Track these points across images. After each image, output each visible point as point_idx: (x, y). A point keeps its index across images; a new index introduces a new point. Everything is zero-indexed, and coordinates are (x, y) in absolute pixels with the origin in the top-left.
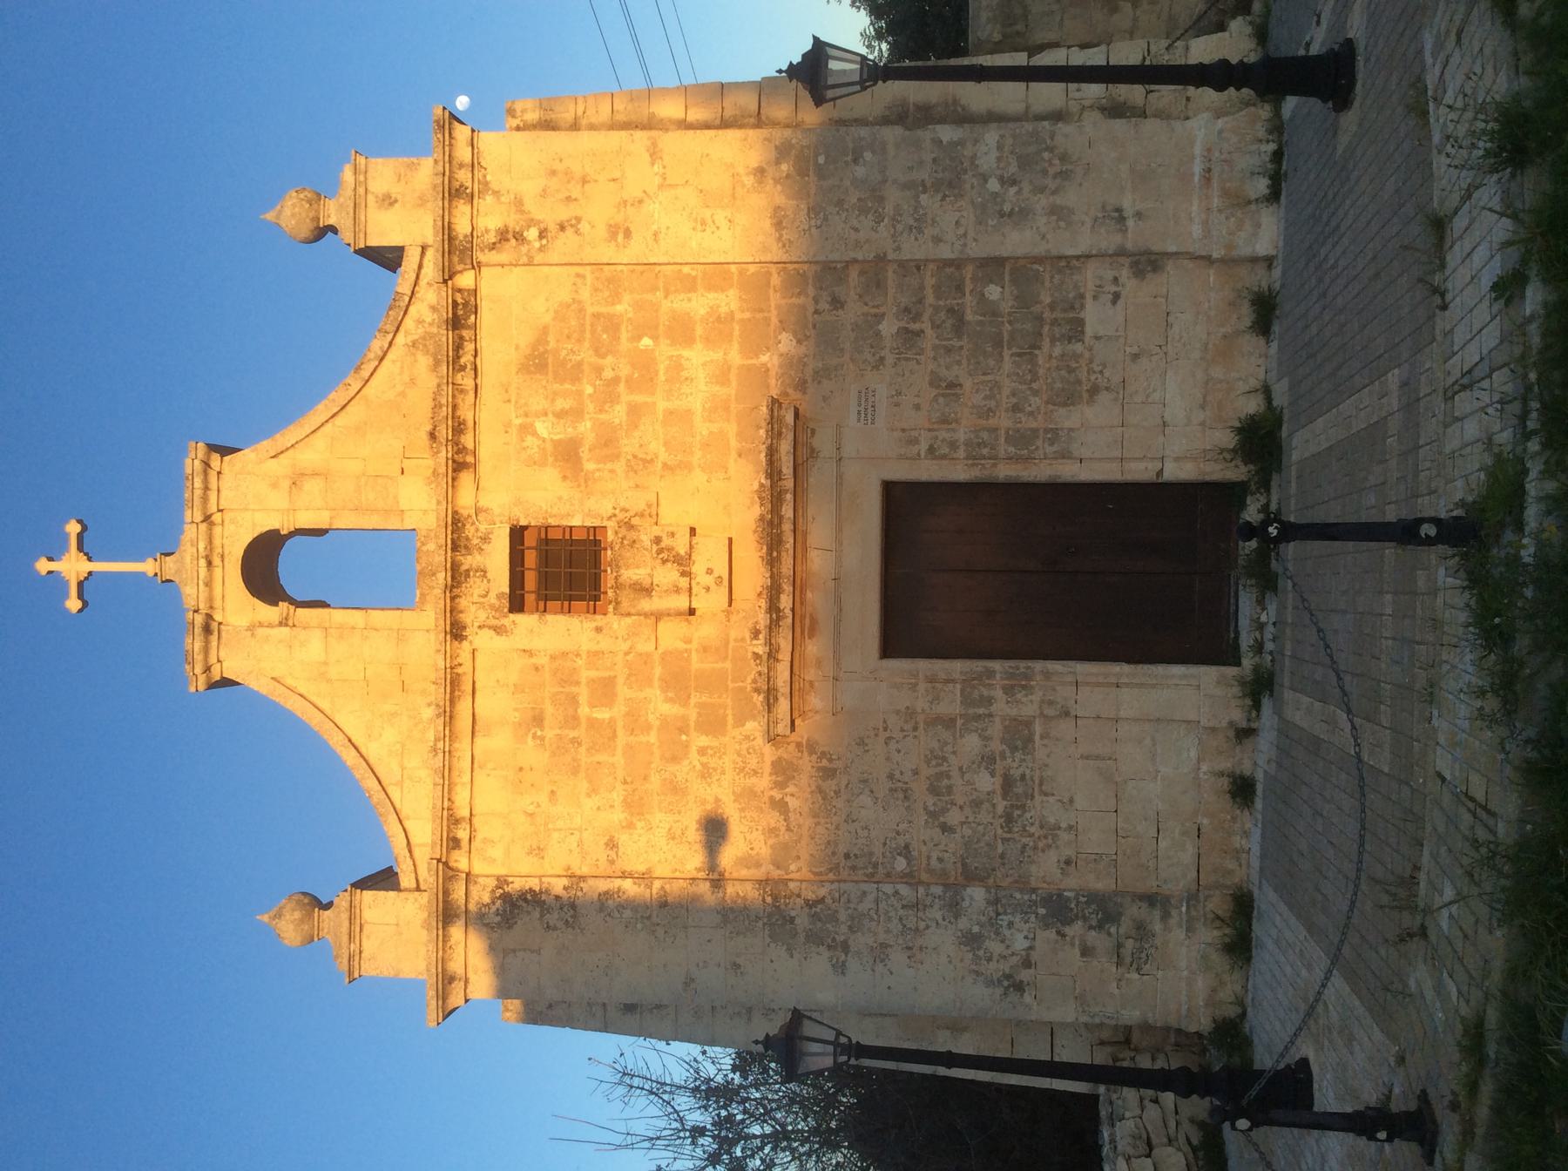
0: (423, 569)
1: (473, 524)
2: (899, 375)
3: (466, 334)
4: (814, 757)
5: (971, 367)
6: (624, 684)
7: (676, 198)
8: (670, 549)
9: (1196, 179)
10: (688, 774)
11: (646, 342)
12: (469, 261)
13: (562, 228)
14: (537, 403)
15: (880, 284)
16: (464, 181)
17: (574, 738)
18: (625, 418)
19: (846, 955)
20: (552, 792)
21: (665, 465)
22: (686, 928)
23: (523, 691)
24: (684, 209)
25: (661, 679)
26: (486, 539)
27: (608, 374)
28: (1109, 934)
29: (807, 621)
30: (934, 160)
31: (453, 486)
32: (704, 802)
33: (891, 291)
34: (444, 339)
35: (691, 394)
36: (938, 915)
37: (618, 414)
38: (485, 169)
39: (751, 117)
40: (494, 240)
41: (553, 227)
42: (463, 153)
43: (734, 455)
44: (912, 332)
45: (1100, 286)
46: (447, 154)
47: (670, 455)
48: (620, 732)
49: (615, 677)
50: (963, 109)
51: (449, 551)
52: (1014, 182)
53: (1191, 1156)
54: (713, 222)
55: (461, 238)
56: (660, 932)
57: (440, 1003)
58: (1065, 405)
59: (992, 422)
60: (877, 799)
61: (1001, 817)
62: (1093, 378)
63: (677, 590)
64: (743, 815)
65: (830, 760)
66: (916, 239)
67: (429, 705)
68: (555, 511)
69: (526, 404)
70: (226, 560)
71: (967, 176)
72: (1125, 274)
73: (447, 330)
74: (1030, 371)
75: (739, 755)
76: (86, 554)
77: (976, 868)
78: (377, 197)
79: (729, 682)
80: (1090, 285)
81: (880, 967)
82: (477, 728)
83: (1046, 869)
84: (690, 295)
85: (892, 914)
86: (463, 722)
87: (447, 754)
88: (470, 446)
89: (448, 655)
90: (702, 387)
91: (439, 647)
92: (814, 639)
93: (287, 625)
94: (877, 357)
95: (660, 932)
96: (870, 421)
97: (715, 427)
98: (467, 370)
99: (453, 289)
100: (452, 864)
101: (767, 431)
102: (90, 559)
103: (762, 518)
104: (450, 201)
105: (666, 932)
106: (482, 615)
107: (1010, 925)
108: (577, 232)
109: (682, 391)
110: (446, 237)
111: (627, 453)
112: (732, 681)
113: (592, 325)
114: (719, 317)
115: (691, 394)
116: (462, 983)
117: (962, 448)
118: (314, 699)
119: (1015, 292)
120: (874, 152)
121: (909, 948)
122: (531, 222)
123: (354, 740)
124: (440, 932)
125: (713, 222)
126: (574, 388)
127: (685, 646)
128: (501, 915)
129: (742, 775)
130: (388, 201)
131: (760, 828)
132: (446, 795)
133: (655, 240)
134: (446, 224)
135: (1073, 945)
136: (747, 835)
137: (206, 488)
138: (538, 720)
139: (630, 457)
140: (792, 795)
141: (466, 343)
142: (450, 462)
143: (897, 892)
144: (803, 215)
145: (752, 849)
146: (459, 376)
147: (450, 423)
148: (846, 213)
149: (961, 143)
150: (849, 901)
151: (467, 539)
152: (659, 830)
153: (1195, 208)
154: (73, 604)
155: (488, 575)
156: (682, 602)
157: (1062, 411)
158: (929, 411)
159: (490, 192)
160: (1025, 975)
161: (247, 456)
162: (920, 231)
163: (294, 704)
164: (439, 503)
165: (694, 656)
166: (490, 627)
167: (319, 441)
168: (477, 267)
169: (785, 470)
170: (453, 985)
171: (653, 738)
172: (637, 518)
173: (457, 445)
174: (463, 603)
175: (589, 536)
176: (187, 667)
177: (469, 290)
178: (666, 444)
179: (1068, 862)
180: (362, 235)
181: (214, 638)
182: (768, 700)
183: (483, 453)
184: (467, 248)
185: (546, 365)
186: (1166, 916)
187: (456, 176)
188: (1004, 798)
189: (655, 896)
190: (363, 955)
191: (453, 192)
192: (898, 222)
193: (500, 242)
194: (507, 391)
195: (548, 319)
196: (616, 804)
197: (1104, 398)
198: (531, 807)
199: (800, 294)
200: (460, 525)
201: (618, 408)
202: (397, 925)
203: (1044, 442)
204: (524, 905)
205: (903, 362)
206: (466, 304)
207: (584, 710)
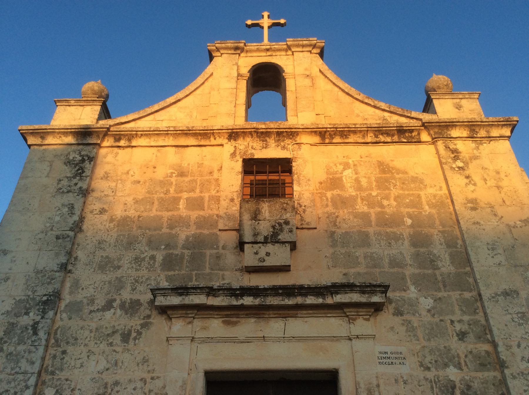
4: (139, 327)
8: (282, 230)
10: (139, 250)
12: (436, 136)
13: (467, 177)
15: (483, 366)
17: (170, 191)
23: (198, 167)
25: (201, 233)
26: (284, 148)
31: (312, 132)
33: (479, 374)
35: (381, 246)
38: (489, 143)
41: (467, 173)
42: (495, 132)
46: (493, 123)
49: (204, 210)
51: (277, 130)
54: (496, 255)
56: (41, 236)
64: (107, 283)
68: (301, 178)
73: (397, 127)
75: (147, 279)
79: (196, 272)
84: (444, 244)
85: (13, 385)
86: (183, 141)
87: (167, 132)
88: (335, 141)
89: (220, 131)
90: (386, 252)
93: (238, 76)
94: (430, 365)
95: (41, 236)
97: (361, 260)
98: (376, 139)
99: (420, 129)
100: (106, 138)
105: (40, 239)
108: (467, 184)
111: (339, 212)
112: (196, 274)
113: (412, 194)
123: (179, 102)
124: (69, 130)
125: (496, 255)
126: (374, 186)
128: (73, 159)
129: (133, 281)
131: (95, 294)
132: (144, 133)
136: (93, 286)
137: (303, 46)
140: (114, 314)
141: (390, 138)
142: (325, 130)
146: (372, 135)
150: (30, 352)
151: (283, 141)
154: (249, 22)
155: (264, 149)
161: (320, 62)
163: (200, 80)
164: (303, 125)
165: (215, 251)
167: (330, 86)
170: (39, 139)
172: (300, 218)
173: (334, 134)
174: (249, 139)
175: (287, 194)
180: (437, 97)
181: (233, 52)
183: (331, 148)
187: (482, 129)
190: (68, 107)
191: (473, 128)
200: (291, 137)
204: (76, 169)
205: (429, 386)
206: (412, 137)
207: (185, 195)
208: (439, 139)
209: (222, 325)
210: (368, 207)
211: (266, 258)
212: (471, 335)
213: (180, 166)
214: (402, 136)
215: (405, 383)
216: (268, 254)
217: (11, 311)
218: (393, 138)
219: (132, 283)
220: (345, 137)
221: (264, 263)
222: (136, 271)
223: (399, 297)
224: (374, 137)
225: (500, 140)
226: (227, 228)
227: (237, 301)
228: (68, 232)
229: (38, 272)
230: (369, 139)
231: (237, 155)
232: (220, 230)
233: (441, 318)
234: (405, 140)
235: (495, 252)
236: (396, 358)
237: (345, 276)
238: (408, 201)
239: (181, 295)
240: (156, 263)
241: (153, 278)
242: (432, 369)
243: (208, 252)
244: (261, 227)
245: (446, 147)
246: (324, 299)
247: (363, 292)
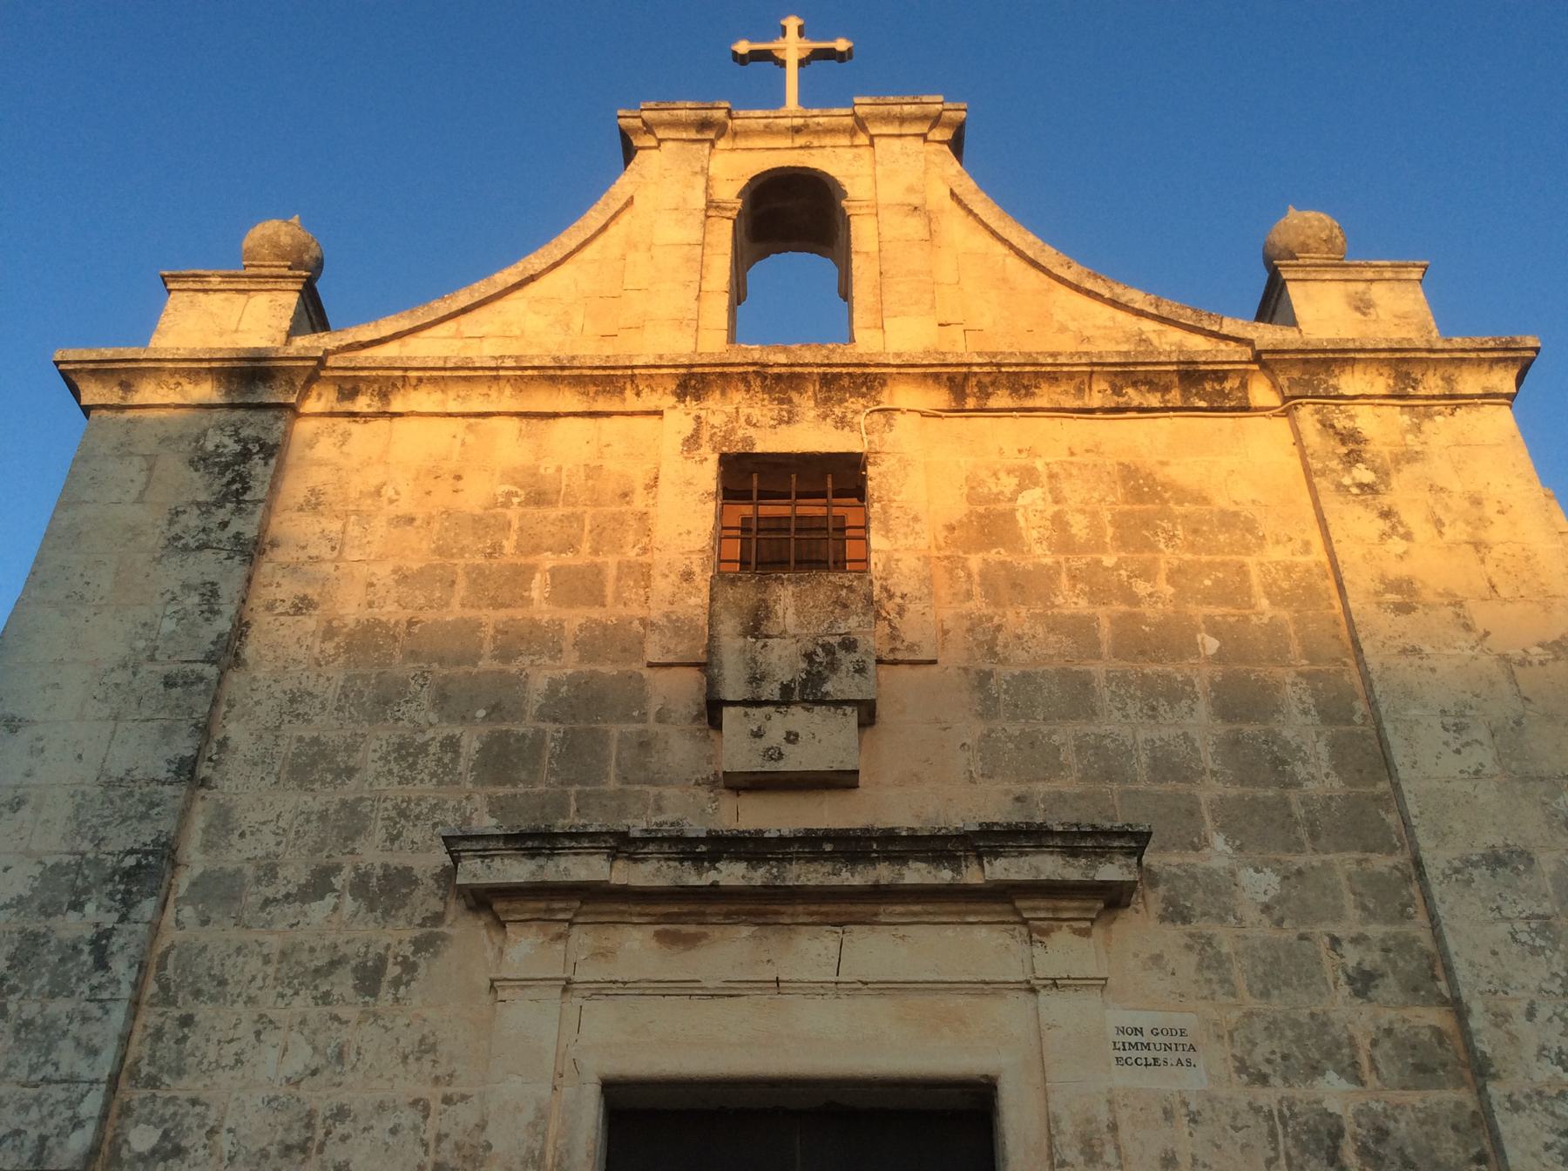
2: (1234, 1118)
4: (408, 950)
8: (833, 666)
12: (1296, 392)
13: (1386, 514)
17: (501, 547)
20: (412, 520)
22: (116, 718)
23: (588, 477)
26: (842, 423)
31: (925, 375)
33: (1414, 1098)
35: (1126, 716)
38: (1452, 414)
40: (1338, 425)
42: (1470, 382)
43: (1020, 789)
44: (1336, 1148)
51: (821, 370)
54: (1467, 744)
55: (1331, 382)
56: (121, 677)
60: (297, 1083)
63: (756, 679)
64: (314, 817)
66: (1548, 1147)
68: (894, 512)
70: (802, 152)
73: (1179, 363)
75: (434, 808)
79: (578, 787)
85: (34, 1114)
86: (542, 400)
87: (494, 373)
88: (993, 403)
90: (1142, 735)
93: (708, 207)
94: (1266, 1069)
95: (121, 677)
96: (1124, 1055)
97: (1068, 756)
98: (1116, 398)
99: (1246, 371)
100: (315, 389)
105: (117, 685)
108: (1384, 536)
111: (1004, 615)
112: (579, 793)
113: (1223, 564)
114: (1284, 762)
116: (116, 401)
118: (600, 240)
122: (1383, 474)
125: (1467, 744)
126: (1108, 540)
129: (393, 814)
132: (428, 374)
136: (272, 826)
140: (335, 909)
142: (965, 370)
143: (77, 1124)
146: (1104, 386)
150: (85, 1019)
152: (313, 676)
154: (743, 47)
155: (784, 426)
156: (733, 687)
161: (953, 167)
164: (898, 355)
167: (982, 241)
170: (116, 389)
172: (888, 630)
173: (993, 383)
174: (738, 396)
177: (1247, 399)
180: (1300, 276)
181: (693, 135)
183: (982, 423)
185: (1142, 501)
187: (1430, 373)
190: (200, 295)
191: (1405, 368)
200: (864, 389)
204: (225, 480)
205: (1265, 1129)
206: (1223, 394)
208: (1304, 401)
209: (654, 944)
210: (1090, 602)
211: (787, 749)
212: (1391, 980)
214: (1194, 391)
215: (1193, 1120)
216: (792, 738)
217: (31, 899)
218: (1167, 397)
219: (389, 818)
220: (1023, 391)
221: (782, 763)
223: (1179, 866)
224: (1109, 392)
226: (670, 659)
228: (198, 667)
229: (109, 785)
230: (1096, 400)
232: (651, 665)
233: (1302, 930)
234: (1203, 404)
235: (1465, 738)
236: (1167, 1047)
238: (1208, 582)
239: (533, 856)
241: (451, 804)
242: (1272, 1080)
243: (615, 730)
244: (773, 658)
246: (957, 870)
247: (1073, 852)
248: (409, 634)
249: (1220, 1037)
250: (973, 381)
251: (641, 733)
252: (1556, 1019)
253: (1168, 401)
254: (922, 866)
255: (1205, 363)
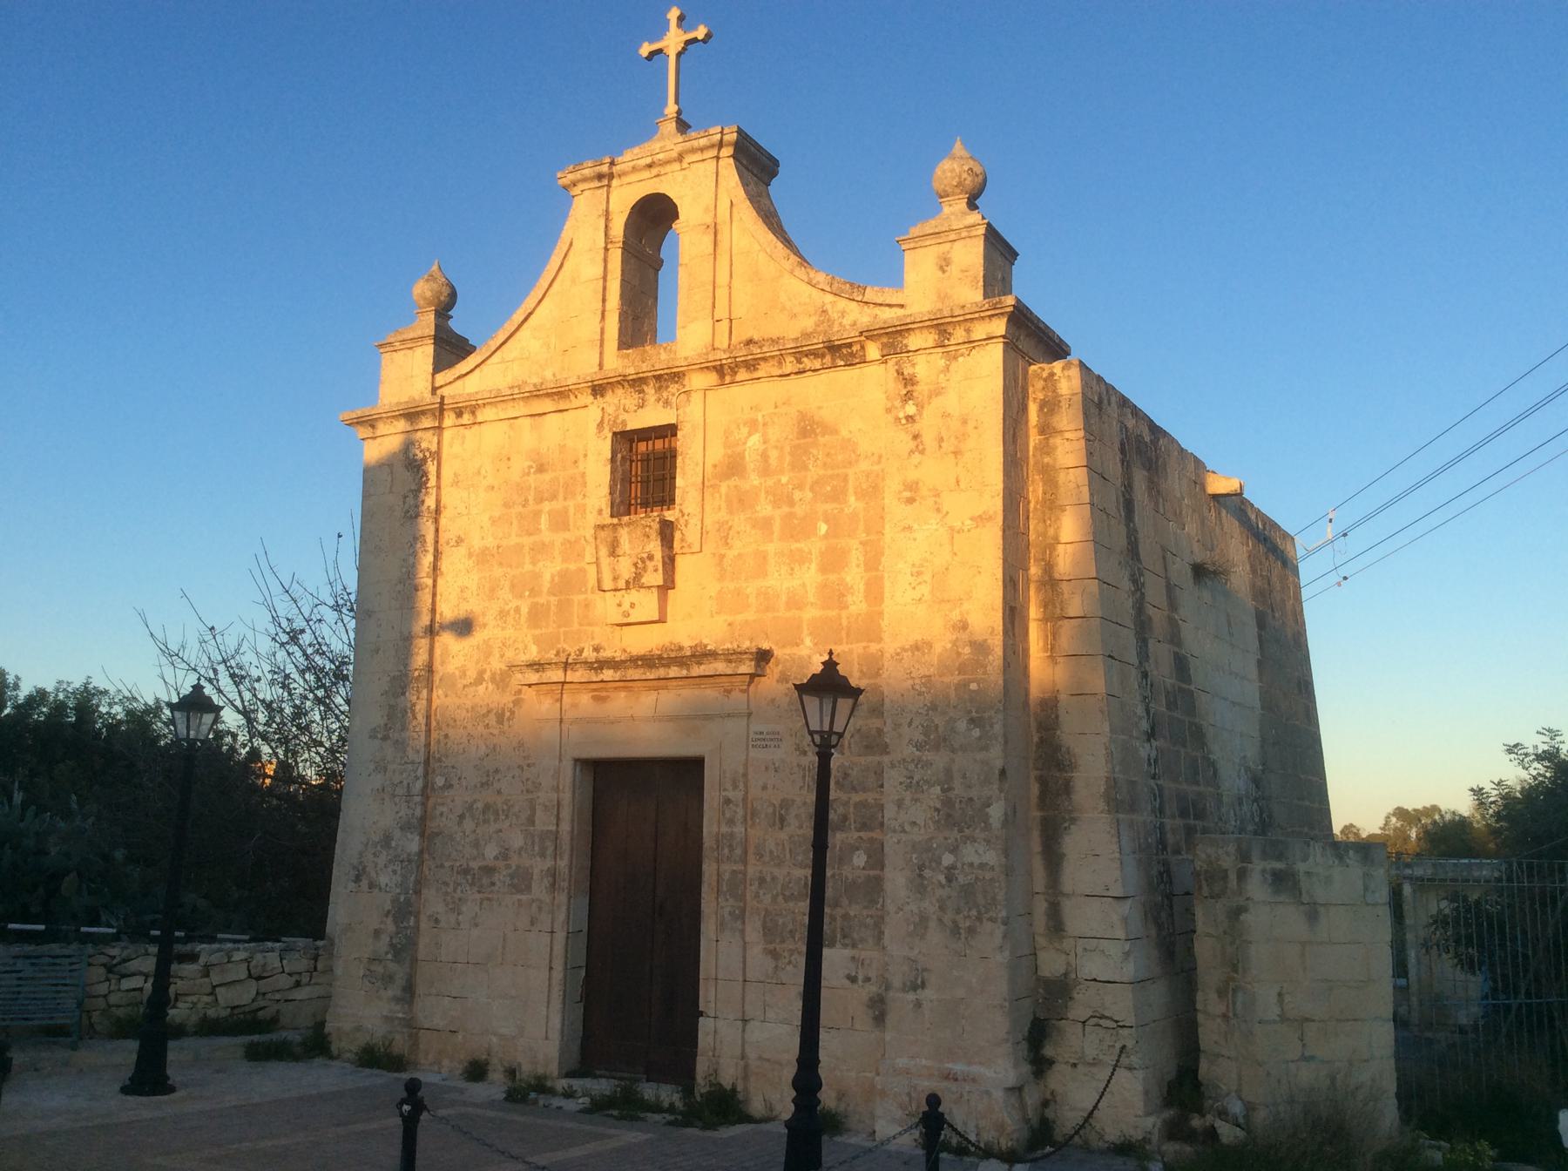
0: (647, 352)
1: (678, 390)
3: (828, 359)
5: (796, 838)
6: (565, 539)
7: (941, 545)
8: (645, 569)
9: (950, 1065)
11: (823, 528)
13: (916, 437)
14: (774, 433)
16: (955, 336)
18: (760, 515)
19: (381, 739)
20: (493, 487)
21: (722, 556)
23: (560, 453)
24: (931, 553)
25: (567, 569)
26: (667, 403)
27: (797, 495)
28: (387, 953)
29: (604, 694)
30: (971, 799)
31: (701, 368)
32: (484, 614)
33: (862, 760)
34: (815, 341)
36: (402, 813)
37: (765, 509)
38: (968, 355)
39: (1062, 610)
40: (905, 373)
42: (980, 331)
43: (730, 619)
45: (862, 964)
47: (731, 560)
48: (532, 539)
49: (569, 530)
50: (1065, 828)
52: (949, 879)
53: (247, 1009)
54: (920, 583)
56: (400, 587)
57: (355, 421)
58: (764, 927)
59: (751, 858)
61: (468, 865)
62: (786, 954)
63: (615, 579)
65: (509, 719)
66: (901, 783)
67: (554, 375)
68: (687, 461)
69: (773, 422)
71: (956, 832)
72: (873, 989)
73: (823, 342)
74: (792, 894)
76: (684, 49)
77: (435, 844)
78: (948, 252)
80: (864, 954)
81: (372, 766)
82: (537, 418)
83: (433, 902)
84: (862, 566)
85: (404, 775)
87: (511, 397)
88: (739, 377)
91: (582, 377)
92: (591, 701)
95: (400, 587)
101: (728, 650)
102: (679, 55)
103: (681, 648)
104: (932, 326)
105: (399, 592)
106: (610, 410)
107: (395, 872)
108: (912, 452)
109: (782, 566)
110: (899, 328)
111: (733, 520)
113: (838, 475)
115: (780, 575)
117: (729, 830)
119: (860, 881)
120: (980, 738)
121: (383, 790)
124: (397, 413)
126: (786, 466)
127: (590, 588)
129: (501, 645)
130: (944, 264)
131: (466, 663)
133: (905, 528)
134: (910, 326)
135: (382, 922)
136: (462, 653)
137: (702, 150)
138: (541, 469)
139: (730, 524)
141: (820, 360)
142: (719, 363)
143: (417, 778)
144: (924, 671)
145: (453, 657)
147: (750, 357)
148: (925, 713)
149: (988, 827)
151: (667, 387)
153: (924, 1062)
154: (645, 50)
155: (640, 409)
157: (759, 924)
158: (762, 798)
159: (948, 362)
160: (364, 883)
162: (909, 786)
164: (686, 359)
165: (583, 597)
166: (603, 417)
168: (884, 359)
169: (702, 667)
171: (528, 567)
172: (681, 535)
174: (620, 391)
176: (572, 167)
177: (865, 356)
178: (740, 555)
179: (437, 921)
180: (912, 245)
182: (535, 664)
183: (735, 389)
184: (895, 349)
185: (805, 437)
186: (397, 1000)
188: (480, 868)
189: (422, 580)
191: (942, 328)
192: (916, 766)
193: (904, 379)
194: (784, 404)
195: (844, 433)
196: (485, 541)
197: (769, 963)
198: (484, 471)
199: (861, 671)
200: (676, 379)
201: (769, 508)
202: (412, 377)
203: (732, 906)
206: (852, 355)
207: (547, 506)
208: (890, 357)
210: (773, 508)
213: (538, 454)
214: (838, 354)
215: (776, 771)
218: (824, 361)
220: (752, 368)
221: (629, 619)
222: (502, 630)
223: (789, 655)
224: (795, 362)
225: (987, 344)
227: (597, 676)
230: (788, 368)
231: (604, 425)
235: (920, 580)
236: (772, 740)
237: (729, 627)
240: (522, 618)
245: (898, 374)
248: (498, 553)
249: (791, 735)
250: (726, 367)
251: (586, 599)
252: (920, 727)
253: (825, 364)
254: (676, 668)
255: (837, 340)
